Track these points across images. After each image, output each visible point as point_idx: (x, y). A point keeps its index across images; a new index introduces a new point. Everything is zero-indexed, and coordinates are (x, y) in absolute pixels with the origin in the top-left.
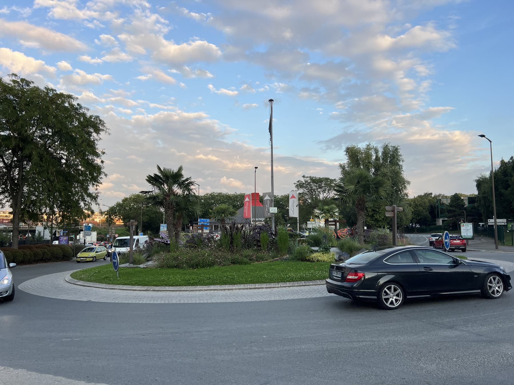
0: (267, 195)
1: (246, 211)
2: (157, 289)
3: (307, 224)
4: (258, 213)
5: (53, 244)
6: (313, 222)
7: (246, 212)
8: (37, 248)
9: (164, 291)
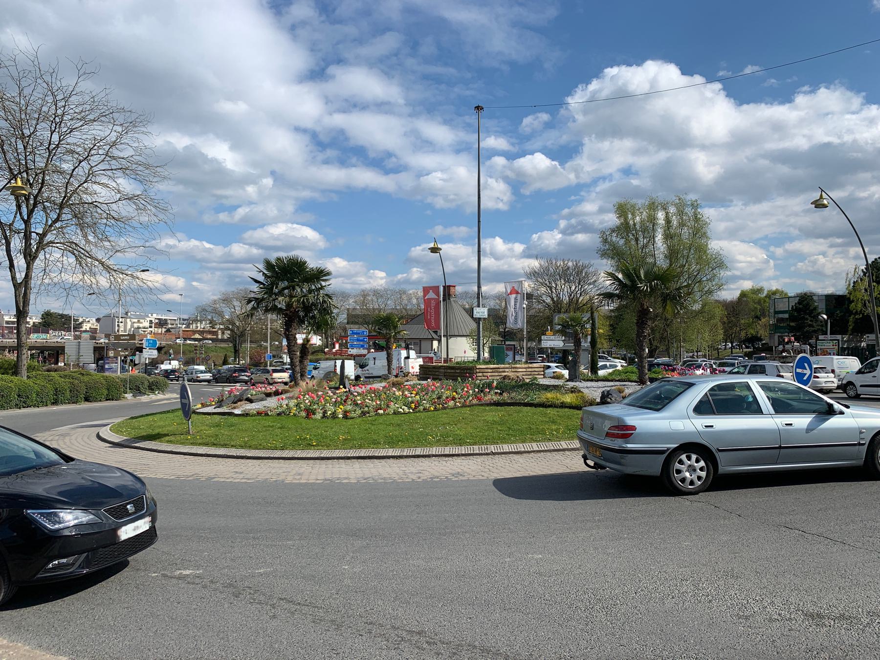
0: (431, 291)
1: (431, 316)
2: (447, 452)
3: (540, 341)
4: (460, 320)
5: (521, 243)
6: (552, 337)
7: (431, 318)
8: (558, 377)
9: (458, 455)
